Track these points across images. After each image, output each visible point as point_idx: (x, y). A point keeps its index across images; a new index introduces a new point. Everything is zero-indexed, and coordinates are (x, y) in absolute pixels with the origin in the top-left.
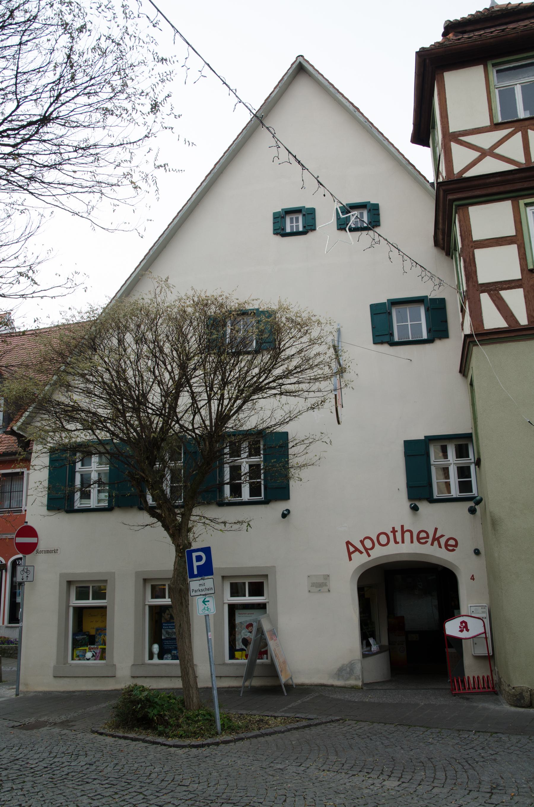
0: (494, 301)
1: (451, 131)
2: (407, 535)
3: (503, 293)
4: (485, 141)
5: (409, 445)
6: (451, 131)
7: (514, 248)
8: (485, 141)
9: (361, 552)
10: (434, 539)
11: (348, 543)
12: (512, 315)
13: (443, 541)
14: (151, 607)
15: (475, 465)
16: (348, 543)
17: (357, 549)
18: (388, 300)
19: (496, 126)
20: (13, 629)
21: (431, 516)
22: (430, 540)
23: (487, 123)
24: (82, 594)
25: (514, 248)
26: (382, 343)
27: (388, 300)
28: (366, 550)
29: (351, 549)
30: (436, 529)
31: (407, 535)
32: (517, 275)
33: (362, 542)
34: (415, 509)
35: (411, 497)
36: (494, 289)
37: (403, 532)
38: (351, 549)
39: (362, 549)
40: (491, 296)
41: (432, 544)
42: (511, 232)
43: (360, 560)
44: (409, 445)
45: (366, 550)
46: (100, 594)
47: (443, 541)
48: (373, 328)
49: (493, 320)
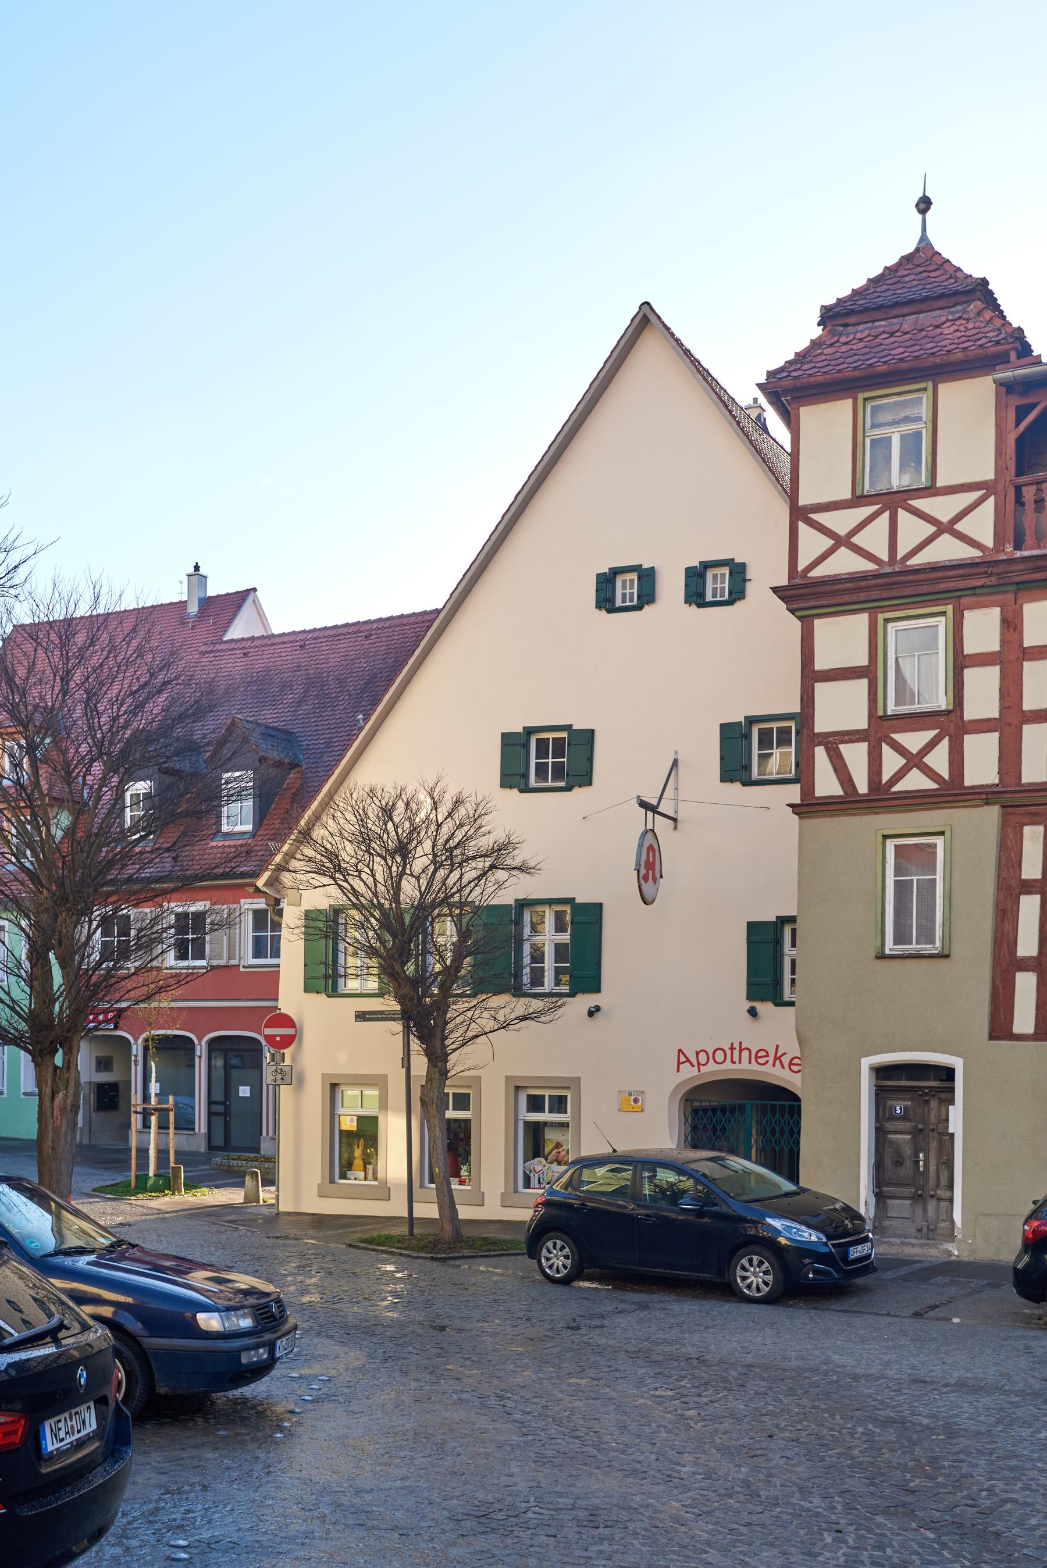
0: (830, 758)
1: (800, 504)
2: (745, 1053)
3: (842, 747)
4: (841, 522)
5: (754, 929)
6: (800, 504)
7: (863, 683)
8: (841, 522)
9: (693, 1066)
10: (776, 1059)
11: (680, 1051)
12: (851, 780)
13: (786, 1060)
14: (527, 1124)
15: (407, 1030)
16: (680, 1051)
17: (688, 1060)
18: (746, 717)
19: (858, 500)
20: (512, 1258)
21: (777, 1027)
22: (771, 1059)
23: (848, 495)
24: (535, 1104)
25: (863, 683)
26: (732, 781)
27: (746, 717)
28: (699, 1064)
29: (682, 1058)
30: (777, 1046)
31: (745, 1053)
32: (863, 724)
33: (697, 1053)
34: (753, 1012)
35: (750, 998)
36: (833, 742)
37: (741, 1051)
38: (682, 1058)
39: (695, 1063)
40: (827, 750)
41: (774, 1065)
42: (863, 661)
43: (688, 1072)
44: (754, 929)
45: (699, 1064)
46: (559, 1104)
47: (786, 1060)
48: (722, 758)
49: (827, 784)
